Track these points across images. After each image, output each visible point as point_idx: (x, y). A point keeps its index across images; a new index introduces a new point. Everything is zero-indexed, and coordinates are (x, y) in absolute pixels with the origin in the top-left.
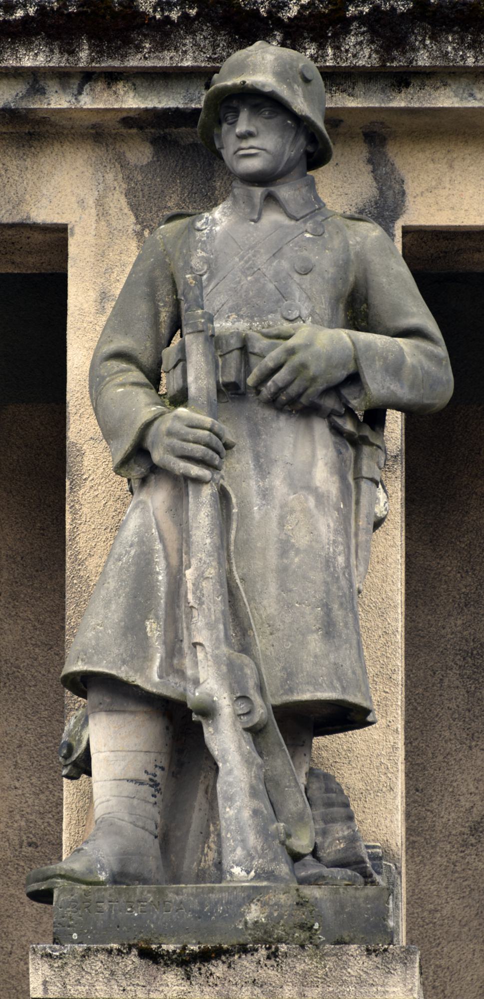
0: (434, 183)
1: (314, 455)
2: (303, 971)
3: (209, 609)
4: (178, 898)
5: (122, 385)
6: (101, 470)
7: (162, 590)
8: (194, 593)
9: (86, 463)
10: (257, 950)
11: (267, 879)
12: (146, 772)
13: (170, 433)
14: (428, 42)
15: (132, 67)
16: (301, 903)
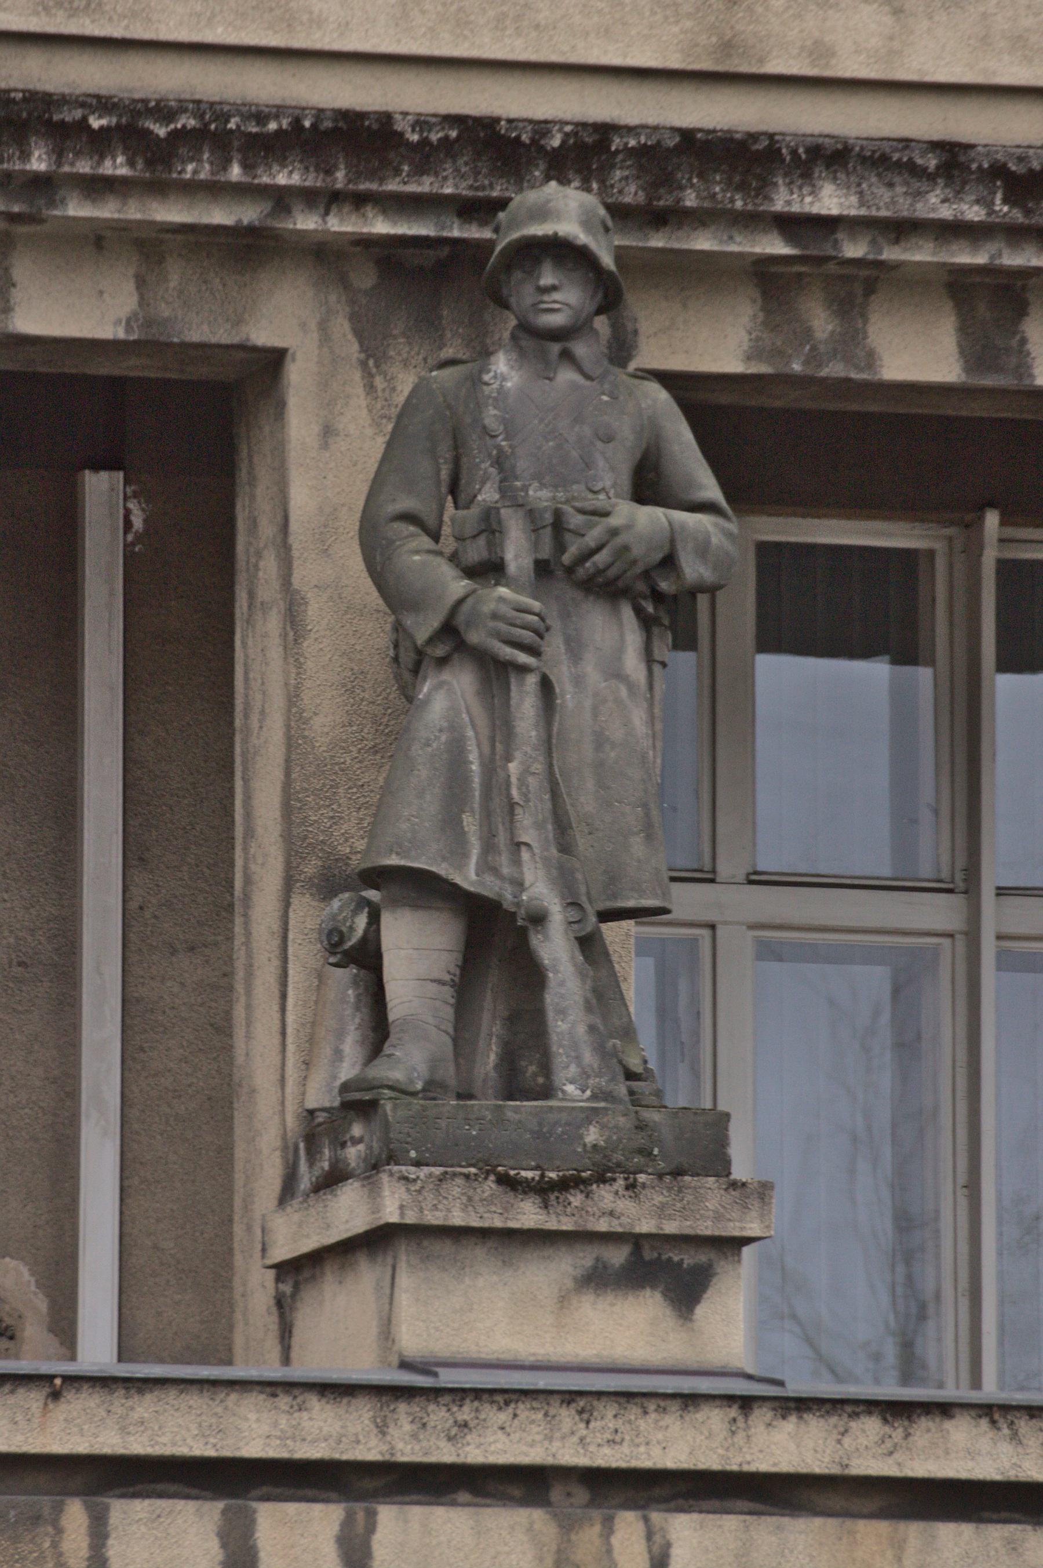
0: (667, 323)
1: (622, 640)
2: (661, 1202)
3: (536, 807)
4: (517, 1117)
5: (417, 552)
6: (326, 621)
7: (476, 782)
8: (519, 789)
9: (310, 613)
10: (614, 1180)
11: (605, 1100)
12: (449, 972)
13: (495, 616)
14: (695, 181)
15: (390, 191)
16: (641, 1126)
